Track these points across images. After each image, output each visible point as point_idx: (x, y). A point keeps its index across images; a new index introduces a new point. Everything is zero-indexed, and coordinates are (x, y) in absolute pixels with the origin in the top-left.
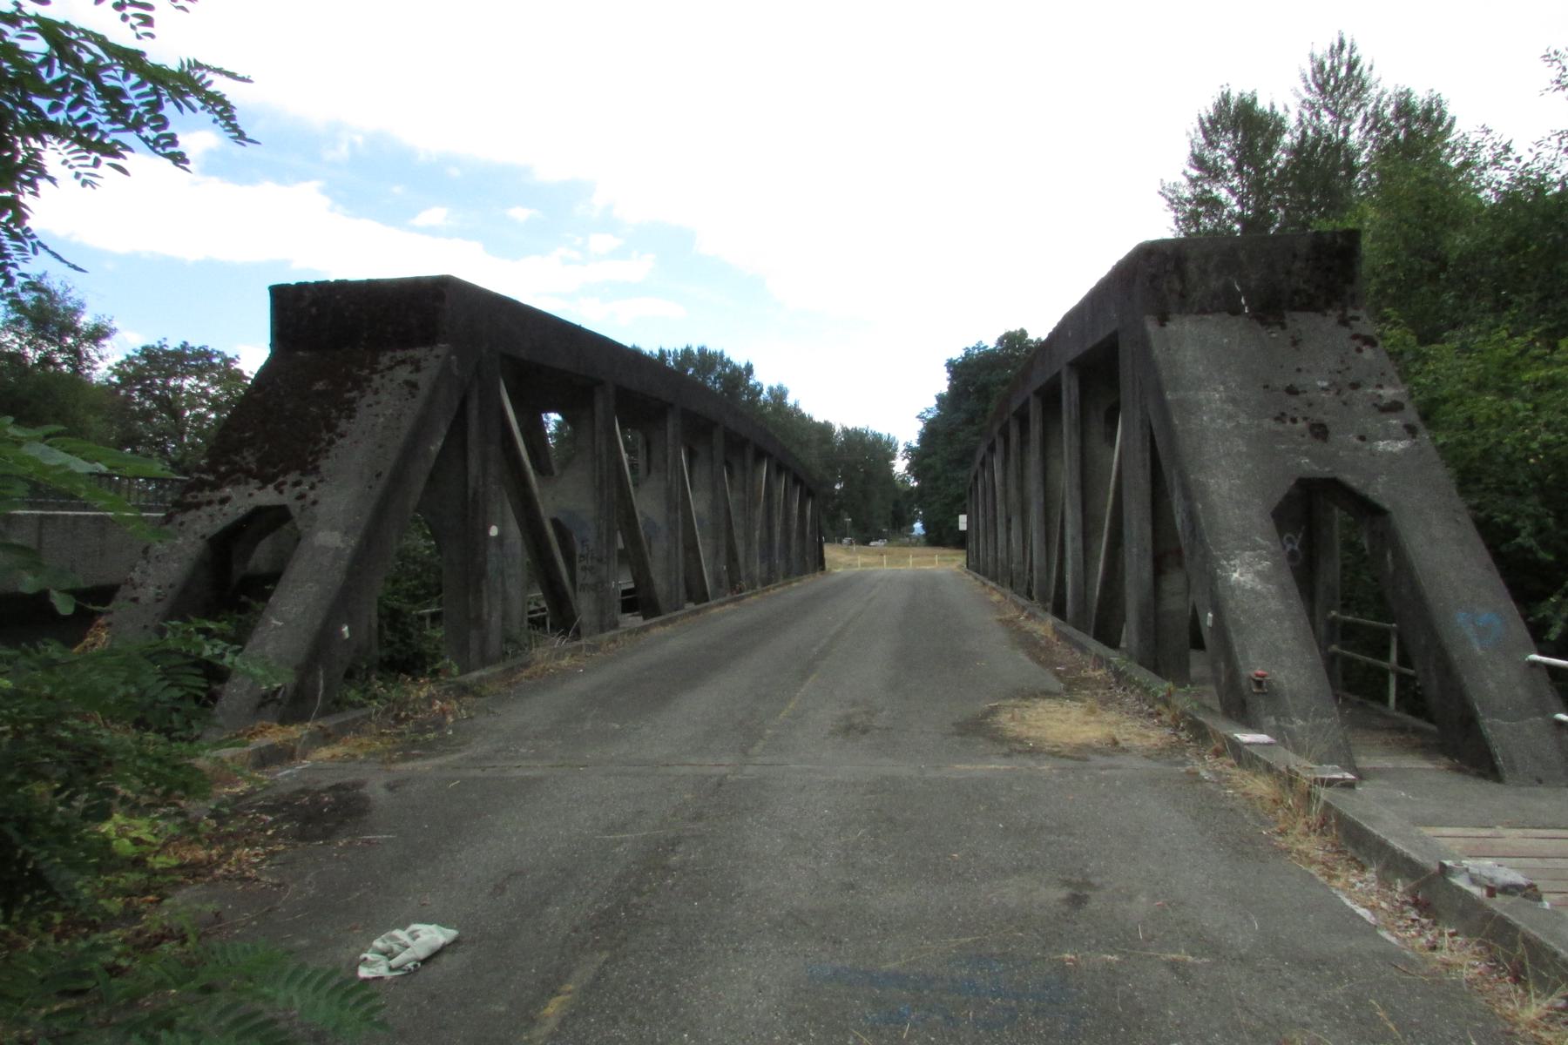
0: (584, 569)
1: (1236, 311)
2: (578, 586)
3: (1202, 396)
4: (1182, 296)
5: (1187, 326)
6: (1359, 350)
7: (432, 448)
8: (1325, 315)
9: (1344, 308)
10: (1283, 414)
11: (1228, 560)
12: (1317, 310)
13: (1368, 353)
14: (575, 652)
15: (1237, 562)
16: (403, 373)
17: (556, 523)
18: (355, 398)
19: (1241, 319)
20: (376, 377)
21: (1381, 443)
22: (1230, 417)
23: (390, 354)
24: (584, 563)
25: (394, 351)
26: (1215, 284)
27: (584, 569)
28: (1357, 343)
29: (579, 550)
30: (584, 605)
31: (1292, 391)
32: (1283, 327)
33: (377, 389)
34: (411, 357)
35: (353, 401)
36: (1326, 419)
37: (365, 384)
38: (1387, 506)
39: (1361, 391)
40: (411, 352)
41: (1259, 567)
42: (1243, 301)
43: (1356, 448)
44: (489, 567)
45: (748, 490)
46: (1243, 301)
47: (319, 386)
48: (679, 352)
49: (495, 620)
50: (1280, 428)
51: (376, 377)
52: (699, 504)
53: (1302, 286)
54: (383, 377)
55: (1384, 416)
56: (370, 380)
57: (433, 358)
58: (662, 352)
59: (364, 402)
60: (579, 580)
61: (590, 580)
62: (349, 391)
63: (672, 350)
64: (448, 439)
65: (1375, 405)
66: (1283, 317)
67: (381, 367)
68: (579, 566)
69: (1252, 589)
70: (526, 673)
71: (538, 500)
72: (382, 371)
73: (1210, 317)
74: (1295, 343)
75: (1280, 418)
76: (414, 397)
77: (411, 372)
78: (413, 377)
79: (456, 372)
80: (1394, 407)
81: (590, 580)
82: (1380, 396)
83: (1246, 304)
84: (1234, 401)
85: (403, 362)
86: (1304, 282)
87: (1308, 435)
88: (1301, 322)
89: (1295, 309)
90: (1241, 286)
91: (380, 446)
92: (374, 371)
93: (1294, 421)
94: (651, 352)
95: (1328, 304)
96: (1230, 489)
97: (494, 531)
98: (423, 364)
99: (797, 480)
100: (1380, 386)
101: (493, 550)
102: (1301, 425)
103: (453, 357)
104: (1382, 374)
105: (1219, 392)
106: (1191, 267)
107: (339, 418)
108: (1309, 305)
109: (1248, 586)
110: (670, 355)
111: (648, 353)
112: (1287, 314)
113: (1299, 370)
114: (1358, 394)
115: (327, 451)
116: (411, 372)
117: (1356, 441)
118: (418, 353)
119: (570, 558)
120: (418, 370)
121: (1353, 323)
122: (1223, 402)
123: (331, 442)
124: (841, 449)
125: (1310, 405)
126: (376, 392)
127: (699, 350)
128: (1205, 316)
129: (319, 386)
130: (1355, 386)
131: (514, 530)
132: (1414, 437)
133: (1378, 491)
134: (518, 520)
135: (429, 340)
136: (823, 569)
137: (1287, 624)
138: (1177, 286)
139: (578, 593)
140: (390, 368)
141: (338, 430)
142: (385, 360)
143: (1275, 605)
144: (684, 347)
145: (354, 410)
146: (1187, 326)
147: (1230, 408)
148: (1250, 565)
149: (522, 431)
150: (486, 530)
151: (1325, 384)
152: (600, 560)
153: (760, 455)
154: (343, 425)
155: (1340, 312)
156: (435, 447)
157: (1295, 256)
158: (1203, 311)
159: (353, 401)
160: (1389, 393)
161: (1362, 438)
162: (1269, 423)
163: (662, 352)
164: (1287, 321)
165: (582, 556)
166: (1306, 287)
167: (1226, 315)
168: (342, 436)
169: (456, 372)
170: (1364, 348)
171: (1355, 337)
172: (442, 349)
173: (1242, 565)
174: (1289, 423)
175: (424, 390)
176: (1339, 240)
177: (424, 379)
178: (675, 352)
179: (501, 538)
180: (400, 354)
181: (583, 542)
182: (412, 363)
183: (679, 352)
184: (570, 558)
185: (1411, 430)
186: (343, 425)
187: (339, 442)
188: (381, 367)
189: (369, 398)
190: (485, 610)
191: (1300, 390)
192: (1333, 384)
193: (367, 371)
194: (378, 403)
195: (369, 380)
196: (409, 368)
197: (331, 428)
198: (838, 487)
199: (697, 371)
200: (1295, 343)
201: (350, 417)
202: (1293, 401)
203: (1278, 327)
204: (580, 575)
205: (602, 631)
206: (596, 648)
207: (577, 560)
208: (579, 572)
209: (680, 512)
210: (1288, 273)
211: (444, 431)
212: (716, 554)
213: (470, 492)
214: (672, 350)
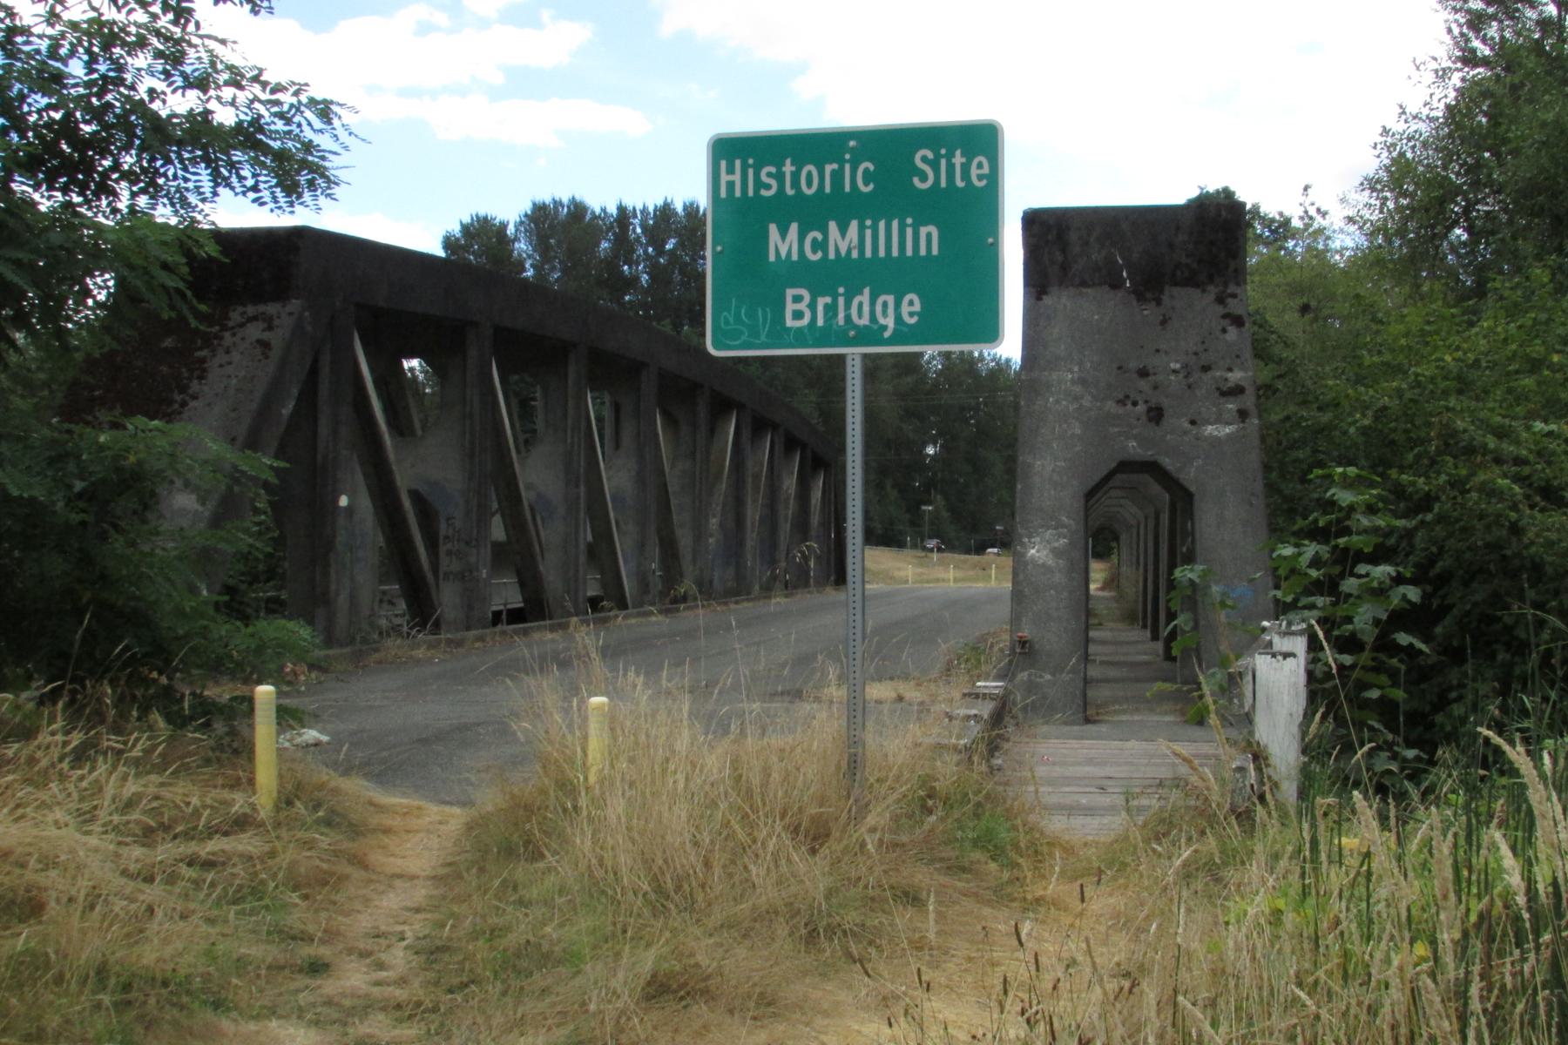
0: (449, 553)
1: (1116, 284)
2: (441, 576)
3: (1055, 376)
4: (1064, 268)
5: (1064, 300)
6: (1224, 331)
7: (44, 206)
8: (1204, 291)
9: (1226, 285)
10: (1127, 397)
11: (1030, 537)
12: (1197, 285)
13: (1232, 333)
14: (431, 646)
15: (1038, 539)
16: (254, 331)
17: (416, 497)
18: (205, 357)
19: (1120, 294)
20: (227, 335)
21: (1210, 427)
22: (1076, 398)
23: (240, 309)
24: (449, 546)
25: (244, 305)
26: (1097, 256)
27: (449, 553)
28: (1226, 322)
29: (443, 529)
30: (448, 598)
31: (1143, 373)
32: (1159, 302)
33: (228, 348)
34: (263, 313)
35: (203, 361)
36: (1165, 402)
37: (215, 342)
38: (1193, 489)
39: (1210, 374)
40: (261, 308)
41: (1056, 545)
42: (1125, 274)
43: (1185, 433)
44: (339, 539)
45: (698, 456)
46: (1125, 274)
47: (168, 343)
48: (651, 209)
49: (342, 601)
50: (1121, 410)
51: (227, 335)
52: (616, 478)
53: (1184, 260)
54: (234, 335)
55: (1222, 400)
56: (222, 338)
57: (286, 314)
58: (622, 209)
59: (217, 361)
60: (443, 568)
61: (456, 566)
62: (201, 349)
63: (639, 207)
64: (299, 400)
65: (1218, 389)
66: (1162, 292)
67: (231, 324)
68: (443, 549)
69: (1044, 565)
70: (376, 656)
71: (394, 468)
72: (233, 328)
73: (1089, 290)
74: (1164, 322)
75: (1121, 402)
76: (267, 358)
77: (264, 330)
78: (266, 336)
79: (309, 328)
80: (1237, 391)
81: (456, 566)
82: (1226, 380)
83: (1129, 277)
84: (1083, 381)
85: (255, 318)
86: (1187, 256)
87: (1144, 418)
88: (1176, 298)
89: (1176, 284)
90: (1123, 259)
91: (234, 410)
92: (224, 328)
93: (1135, 404)
94: (604, 210)
95: (1211, 279)
96: (1053, 471)
97: (344, 501)
98: (276, 322)
99: (791, 443)
100: (1230, 370)
101: (341, 521)
102: (1141, 408)
103: (307, 314)
104: (1238, 356)
105: (1072, 372)
106: (1073, 236)
107: (190, 379)
108: (1192, 281)
109: (1041, 561)
110: (635, 216)
111: (598, 211)
112: (1167, 288)
113: (1158, 351)
114: (1207, 377)
115: (180, 413)
116: (264, 330)
117: (1187, 425)
118: (271, 309)
119: (432, 543)
120: (270, 328)
121: (1230, 300)
122: (1073, 381)
123: (184, 404)
124: (936, 384)
125: (1156, 388)
126: (228, 352)
127: (685, 208)
128: (1084, 290)
129: (168, 343)
130: (1206, 369)
131: (366, 504)
132: (1243, 422)
133: (1189, 476)
134: (369, 488)
135: (281, 296)
136: (840, 579)
137: (1065, 594)
138: (1059, 257)
139: (441, 581)
140: (242, 325)
141: (191, 391)
142: (235, 316)
143: (1058, 578)
144: (660, 202)
145: (205, 370)
146: (1064, 300)
147: (1078, 389)
148: (1048, 542)
149: (375, 382)
150: (336, 500)
151: (1178, 366)
152: (467, 543)
153: (722, 406)
154: (195, 386)
155: (1221, 288)
156: (286, 411)
157: (1178, 228)
158: (1084, 284)
159: (203, 361)
160: (1236, 376)
161: (1193, 422)
162: (1111, 406)
163: (622, 209)
164: (1165, 298)
165: (446, 537)
166: (1189, 261)
167: (1107, 288)
168: (195, 397)
169: (309, 328)
170: (1230, 328)
171: (1225, 316)
172: (295, 304)
173: (1040, 543)
174: (1129, 407)
175: (276, 353)
176: (1224, 213)
177: (277, 338)
178: (644, 211)
179: (350, 510)
180: (251, 310)
181: (448, 519)
182: (264, 320)
183: (651, 209)
184: (432, 543)
185: (1243, 414)
186: (195, 386)
187: (193, 404)
188: (231, 324)
189: (221, 357)
190: (333, 587)
191: (1151, 371)
192: (1185, 366)
193: (217, 328)
194: (230, 363)
195: (216, 337)
196: (261, 325)
197: (183, 389)
198: (930, 450)
199: (681, 245)
200: (1164, 322)
201: (201, 378)
202: (1143, 384)
203: (1154, 303)
204: (445, 563)
205: (468, 628)
206: (460, 644)
207: (441, 541)
208: (442, 555)
209: (582, 489)
210: (1171, 246)
211: (295, 392)
212: (641, 546)
213: (319, 457)
214: (639, 207)
